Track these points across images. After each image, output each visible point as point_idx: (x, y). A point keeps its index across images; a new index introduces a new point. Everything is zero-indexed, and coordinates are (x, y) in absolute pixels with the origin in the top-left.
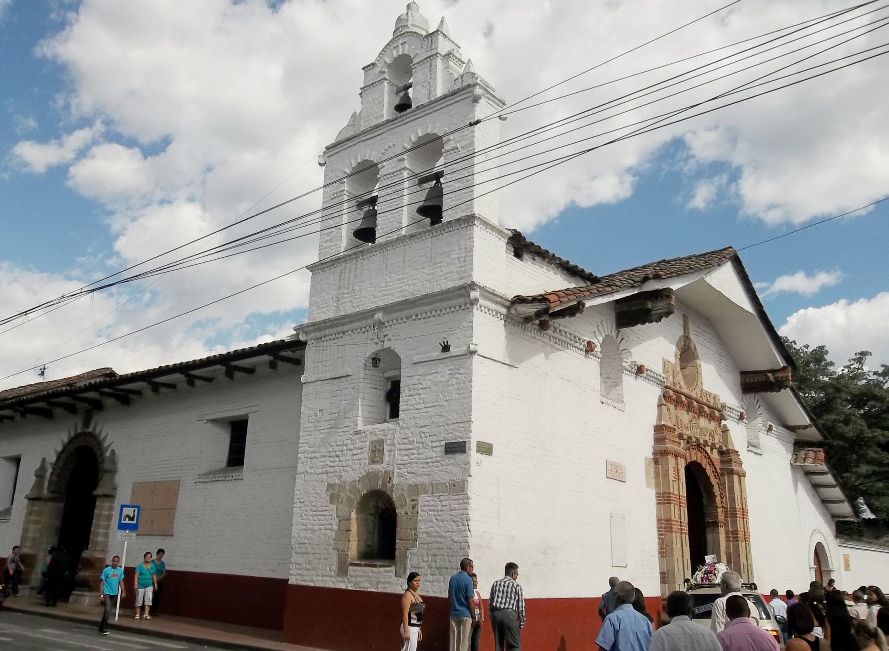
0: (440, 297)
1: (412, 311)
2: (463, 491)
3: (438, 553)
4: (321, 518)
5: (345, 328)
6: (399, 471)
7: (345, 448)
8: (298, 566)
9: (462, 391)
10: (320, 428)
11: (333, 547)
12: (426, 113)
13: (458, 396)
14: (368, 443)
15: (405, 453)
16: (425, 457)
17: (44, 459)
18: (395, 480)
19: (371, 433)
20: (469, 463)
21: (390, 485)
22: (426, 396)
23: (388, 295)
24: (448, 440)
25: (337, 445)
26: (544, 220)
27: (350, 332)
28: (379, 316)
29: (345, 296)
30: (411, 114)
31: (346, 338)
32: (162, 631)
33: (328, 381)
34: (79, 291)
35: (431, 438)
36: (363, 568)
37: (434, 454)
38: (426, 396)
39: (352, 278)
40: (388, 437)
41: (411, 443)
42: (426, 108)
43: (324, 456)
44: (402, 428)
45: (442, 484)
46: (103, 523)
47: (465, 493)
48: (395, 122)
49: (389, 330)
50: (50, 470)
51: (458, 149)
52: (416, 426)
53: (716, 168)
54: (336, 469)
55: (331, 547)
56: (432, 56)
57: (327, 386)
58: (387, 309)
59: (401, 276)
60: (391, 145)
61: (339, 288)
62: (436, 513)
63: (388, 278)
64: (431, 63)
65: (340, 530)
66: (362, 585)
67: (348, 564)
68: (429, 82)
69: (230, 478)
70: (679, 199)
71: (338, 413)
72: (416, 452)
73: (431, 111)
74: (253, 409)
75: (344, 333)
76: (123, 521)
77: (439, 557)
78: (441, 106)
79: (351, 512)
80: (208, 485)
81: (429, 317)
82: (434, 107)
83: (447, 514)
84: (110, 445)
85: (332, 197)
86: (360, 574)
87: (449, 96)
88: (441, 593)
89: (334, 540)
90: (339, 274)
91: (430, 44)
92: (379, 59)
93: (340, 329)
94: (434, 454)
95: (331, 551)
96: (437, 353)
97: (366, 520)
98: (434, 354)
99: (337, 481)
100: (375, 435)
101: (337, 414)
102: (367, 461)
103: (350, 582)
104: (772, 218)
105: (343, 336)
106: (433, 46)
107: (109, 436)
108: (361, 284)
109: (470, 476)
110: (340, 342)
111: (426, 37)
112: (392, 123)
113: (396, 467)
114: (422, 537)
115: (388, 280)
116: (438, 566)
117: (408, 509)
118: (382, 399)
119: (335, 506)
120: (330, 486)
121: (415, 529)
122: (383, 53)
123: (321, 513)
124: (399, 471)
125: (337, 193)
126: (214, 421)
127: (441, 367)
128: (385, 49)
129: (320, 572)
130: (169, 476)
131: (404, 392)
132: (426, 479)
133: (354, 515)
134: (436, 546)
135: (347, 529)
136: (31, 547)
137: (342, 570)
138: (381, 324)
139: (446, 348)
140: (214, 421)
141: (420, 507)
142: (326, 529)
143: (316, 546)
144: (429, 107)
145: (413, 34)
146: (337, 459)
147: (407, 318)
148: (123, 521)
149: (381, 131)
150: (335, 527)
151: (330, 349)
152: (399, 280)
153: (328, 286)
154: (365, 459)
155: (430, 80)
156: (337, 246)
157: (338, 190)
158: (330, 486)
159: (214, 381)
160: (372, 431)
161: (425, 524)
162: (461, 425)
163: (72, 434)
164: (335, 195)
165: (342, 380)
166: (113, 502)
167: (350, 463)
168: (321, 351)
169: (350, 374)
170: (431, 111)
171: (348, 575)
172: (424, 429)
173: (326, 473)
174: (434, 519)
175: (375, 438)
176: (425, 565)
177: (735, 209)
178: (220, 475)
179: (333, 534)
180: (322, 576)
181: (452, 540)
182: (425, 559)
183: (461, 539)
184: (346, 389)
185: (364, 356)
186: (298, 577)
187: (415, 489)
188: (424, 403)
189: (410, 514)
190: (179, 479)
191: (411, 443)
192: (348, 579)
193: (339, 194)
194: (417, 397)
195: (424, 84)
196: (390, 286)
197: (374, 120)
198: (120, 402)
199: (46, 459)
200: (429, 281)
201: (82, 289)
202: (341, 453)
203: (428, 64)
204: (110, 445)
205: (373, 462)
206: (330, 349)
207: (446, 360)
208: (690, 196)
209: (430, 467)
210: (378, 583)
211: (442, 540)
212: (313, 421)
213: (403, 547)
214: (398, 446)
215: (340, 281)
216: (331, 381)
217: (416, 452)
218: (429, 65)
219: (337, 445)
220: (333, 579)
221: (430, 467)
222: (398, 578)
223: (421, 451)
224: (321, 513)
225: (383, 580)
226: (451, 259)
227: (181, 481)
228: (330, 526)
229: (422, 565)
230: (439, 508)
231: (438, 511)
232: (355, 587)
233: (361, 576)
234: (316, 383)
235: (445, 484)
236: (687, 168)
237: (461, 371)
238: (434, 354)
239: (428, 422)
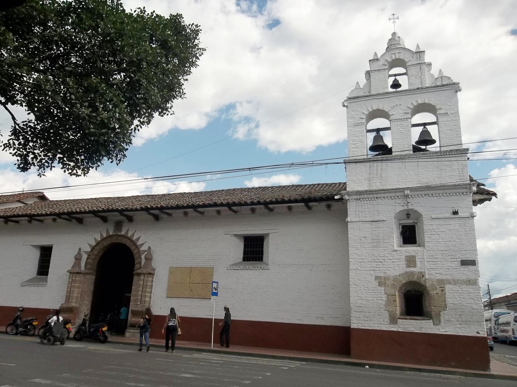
0: (452, 187)
1: (430, 192)
2: (477, 284)
3: (463, 314)
4: (372, 293)
5: (379, 196)
6: (429, 272)
7: (386, 258)
8: (357, 319)
9: (468, 235)
10: (365, 247)
11: (384, 309)
12: (422, 92)
13: (466, 237)
14: (404, 257)
15: (432, 263)
16: (447, 266)
17: (80, 249)
18: (427, 277)
19: (405, 251)
20: (478, 271)
21: (424, 279)
22: (444, 236)
23: (408, 182)
24: (462, 259)
25: (379, 256)
26: (160, 132)
27: (382, 198)
28: (407, 192)
29: (375, 179)
30: (413, 91)
31: (379, 201)
32: (245, 352)
33: (368, 222)
34: (311, 163)
35: (450, 257)
36: (409, 321)
37: (453, 265)
38: (444, 236)
39: (379, 170)
40: (419, 255)
41: (436, 258)
42: (423, 90)
43: (371, 262)
44: (428, 250)
45: (461, 280)
46: (148, 290)
47: (478, 285)
48: (400, 93)
49: (412, 200)
50: (85, 257)
51: (448, 114)
52: (438, 250)
53: (247, 120)
54: (381, 268)
55: (383, 309)
56: (422, 63)
57: (368, 225)
58: (411, 189)
59: (417, 173)
60: (398, 104)
61: (370, 174)
62: (459, 294)
63: (407, 173)
64: (420, 67)
65: (389, 301)
66: (409, 329)
67: (397, 318)
68: (420, 76)
69: (256, 268)
70: (230, 132)
71: (378, 239)
72: (440, 263)
73: (426, 91)
74: (273, 231)
75: (377, 198)
76: (213, 291)
77: (464, 316)
78: (434, 90)
79: (395, 291)
80: (240, 271)
81: (441, 196)
82: (429, 90)
83: (466, 295)
84: (143, 244)
85: (355, 125)
86: (408, 323)
87: (440, 86)
88: (467, 333)
89: (385, 305)
90: (369, 167)
91: (419, 57)
92: (381, 57)
93: (375, 196)
94: (453, 265)
95: (383, 311)
96: (449, 215)
97: (400, 295)
98: (447, 215)
99: (382, 275)
100: (409, 253)
101: (377, 240)
102: (405, 266)
103: (399, 327)
104: (272, 148)
105: (377, 199)
106: (421, 58)
107: (141, 237)
108: (387, 174)
109: (479, 277)
110: (375, 202)
111: (416, 53)
112: (398, 93)
113: (427, 270)
114: (449, 306)
115: (407, 174)
116: (463, 320)
117: (438, 291)
118: (399, 234)
119: (383, 288)
120: (377, 278)
121: (445, 301)
122: (384, 55)
123: (372, 291)
124: (429, 272)
125: (359, 123)
126: (236, 235)
127: (452, 222)
128: (386, 53)
129: (376, 322)
130: (202, 265)
131: (427, 232)
132: (449, 277)
133: (397, 293)
134: (461, 310)
135: (394, 300)
136: (76, 303)
137: (393, 320)
138: (407, 196)
139: (455, 213)
140: (236, 235)
141: (446, 291)
142: (377, 300)
143: (371, 308)
144: (425, 89)
145: (411, 52)
146: (381, 264)
147: (425, 195)
148: (213, 291)
149: (390, 96)
150: (385, 299)
151: (367, 205)
152: (416, 175)
153: (361, 172)
154: (403, 265)
155: (421, 75)
156: (363, 152)
157: (359, 122)
158: (377, 278)
159: (239, 213)
160: (406, 250)
161: (452, 299)
162: (471, 252)
163: (105, 235)
164: (357, 124)
165: (379, 222)
166: (153, 278)
167: (392, 266)
168: (360, 206)
169: (385, 220)
170: (426, 91)
171: (398, 324)
172: (444, 252)
173: (373, 270)
174: (457, 297)
175: (409, 254)
176: (454, 320)
177: (256, 141)
178: (250, 266)
179: (384, 302)
180: (378, 324)
181: (472, 308)
182: (454, 316)
183: (478, 308)
184: (383, 227)
185: (395, 212)
186: (358, 324)
187: (442, 282)
188: (442, 239)
189: (440, 294)
190: (213, 267)
191: (436, 258)
192: (398, 326)
193: (360, 124)
194: (437, 236)
195: (417, 77)
196: (409, 177)
197: (381, 89)
198: (154, 219)
199: (82, 249)
200: (438, 178)
201: (313, 161)
202: (383, 260)
203: (419, 67)
204: (143, 244)
205: (408, 266)
206: (367, 205)
207: (456, 219)
208: (235, 131)
209: (451, 271)
210: (421, 328)
211: (465, 308)
212: (359, 242)
213: (437, 310)
214: (426, 260)
215: (370, 170)
216: (371, 223)
217: (440, 263)
218: (419, 68)
219: (379, 256)
220: (387, 326)
221: (451, 271)
222: (435, 326)
223: (443, 263)
224: (372, 291)
225: (424, 327)
226: (452, 169)
227: (215, 268)
228: (381, 298)
229: (452, 319)
230: (460, 292)
231: (460, 293)
232: (404, 330)
233: (408, 325)
234: (358, 223)
235: (463, 280)
236: (235, 118)
237: (467, 225)
238: (447, 215)
239: (446, 249)
